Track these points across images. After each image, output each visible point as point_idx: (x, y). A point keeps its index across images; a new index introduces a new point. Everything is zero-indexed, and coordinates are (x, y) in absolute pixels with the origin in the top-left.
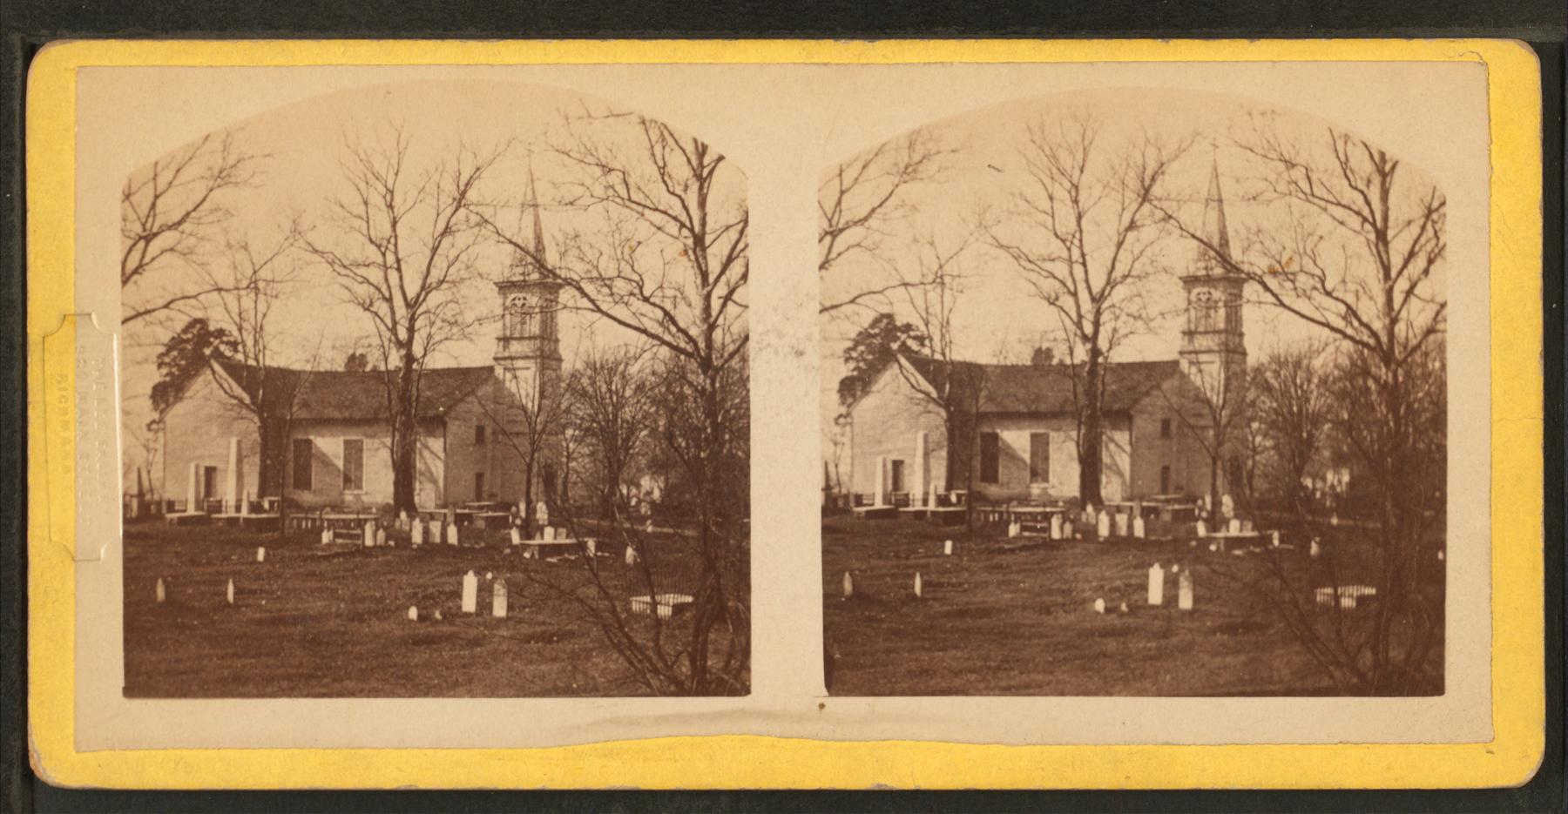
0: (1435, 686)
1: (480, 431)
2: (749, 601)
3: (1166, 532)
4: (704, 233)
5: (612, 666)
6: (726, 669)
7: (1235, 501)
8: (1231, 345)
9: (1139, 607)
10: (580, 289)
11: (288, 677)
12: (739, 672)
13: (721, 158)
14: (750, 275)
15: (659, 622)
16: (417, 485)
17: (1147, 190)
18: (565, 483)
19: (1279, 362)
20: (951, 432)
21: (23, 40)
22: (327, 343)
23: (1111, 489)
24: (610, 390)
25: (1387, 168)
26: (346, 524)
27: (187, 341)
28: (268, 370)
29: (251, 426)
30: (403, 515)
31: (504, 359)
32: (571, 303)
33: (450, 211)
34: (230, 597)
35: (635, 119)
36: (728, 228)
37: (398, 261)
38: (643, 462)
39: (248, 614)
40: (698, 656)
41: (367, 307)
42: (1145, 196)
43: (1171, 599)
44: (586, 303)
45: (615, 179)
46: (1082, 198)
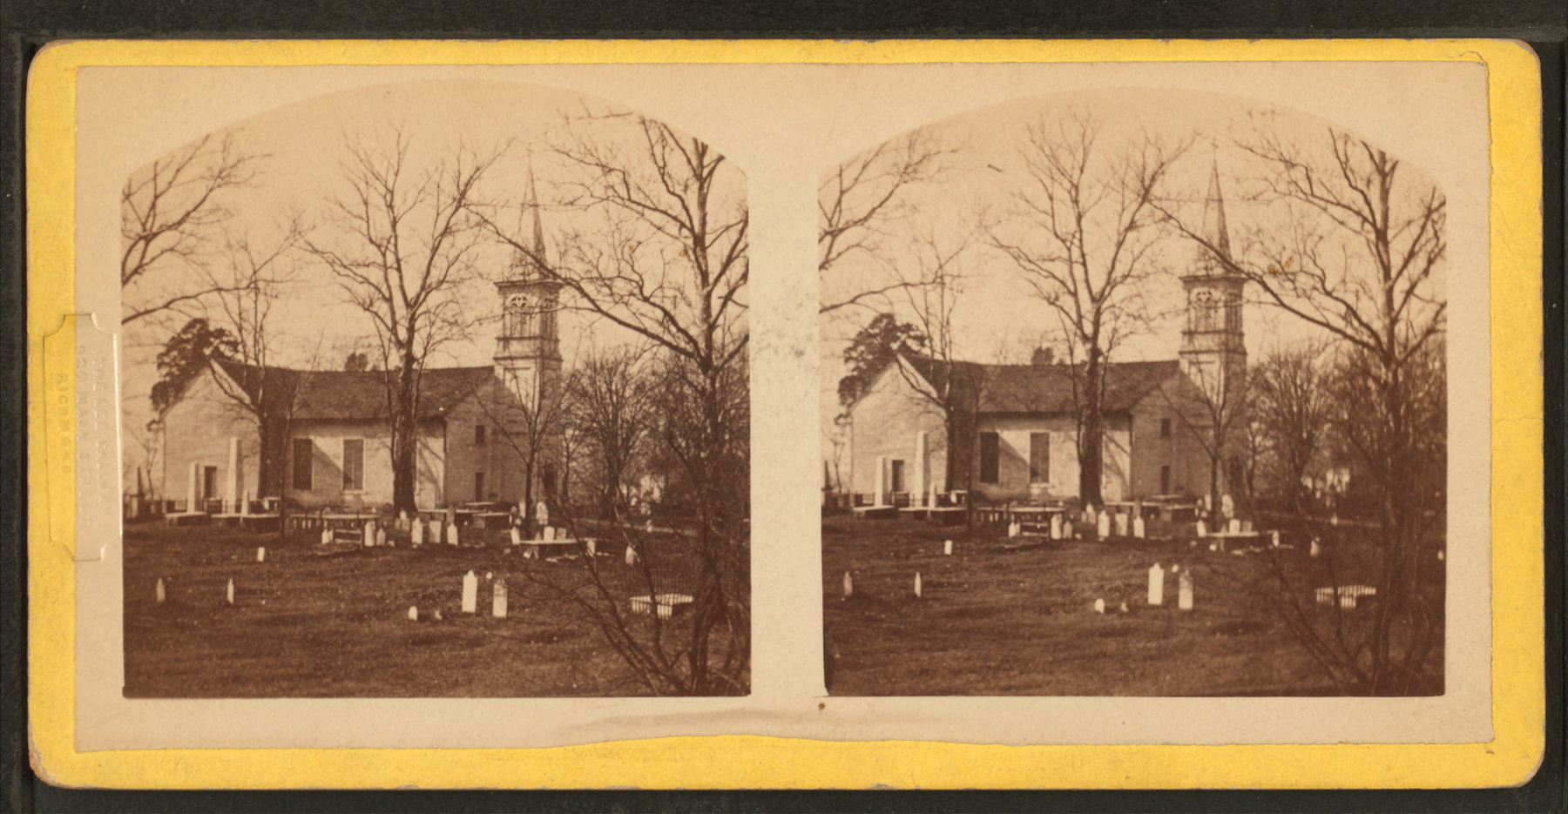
0: (1435, 686)
1: (480, 431)
2: (749, 601)
3: (1166, 533)
4: (704, 233)
5: (612, 666)
6: (726, 669)
7: (1235, 501)
8: (1231, 345)
9: (1139, 607)
10: (580, 289)
11: (288, 678)
12: (739, 672)
13: (721, 158)
14: (750, 276)
15: (659, 622)
16: (417, 485)
17: (1147, 190)
18: (565, 483)
19: (1279, 362)
20: (951, 431)
21: (23, 40)
22: (326, 343)
23: (1111, 489)
24: (610, 390)
25: (1387, 168)
26: (346, 524)
27: (187, 341)
28: (268, 369)
29: (251, 426)
30: (403, 515)
31: (505, 359)
32: (571, 303)
33: (1134, 206)
34: (230, 597)
35: (635, 119)
36: (728, 228)
37: (398, 261)
38: (643, 462)
39: (248, 614)
40: (698, 655)
41: (367, 307)
42: (1145, 196)
43: (1171, 599)
44: (585, 303)
45: (615, 179)
46: (1081, 198)
